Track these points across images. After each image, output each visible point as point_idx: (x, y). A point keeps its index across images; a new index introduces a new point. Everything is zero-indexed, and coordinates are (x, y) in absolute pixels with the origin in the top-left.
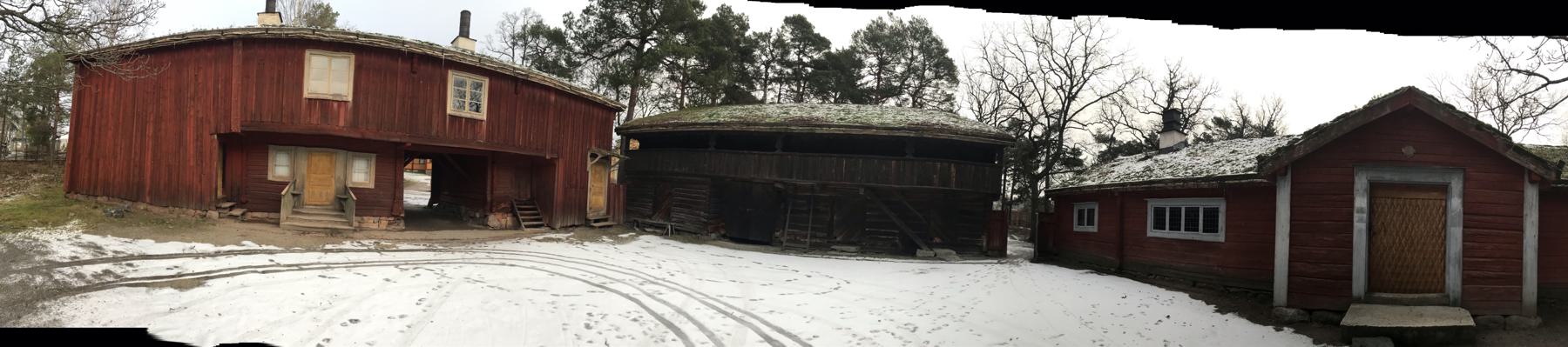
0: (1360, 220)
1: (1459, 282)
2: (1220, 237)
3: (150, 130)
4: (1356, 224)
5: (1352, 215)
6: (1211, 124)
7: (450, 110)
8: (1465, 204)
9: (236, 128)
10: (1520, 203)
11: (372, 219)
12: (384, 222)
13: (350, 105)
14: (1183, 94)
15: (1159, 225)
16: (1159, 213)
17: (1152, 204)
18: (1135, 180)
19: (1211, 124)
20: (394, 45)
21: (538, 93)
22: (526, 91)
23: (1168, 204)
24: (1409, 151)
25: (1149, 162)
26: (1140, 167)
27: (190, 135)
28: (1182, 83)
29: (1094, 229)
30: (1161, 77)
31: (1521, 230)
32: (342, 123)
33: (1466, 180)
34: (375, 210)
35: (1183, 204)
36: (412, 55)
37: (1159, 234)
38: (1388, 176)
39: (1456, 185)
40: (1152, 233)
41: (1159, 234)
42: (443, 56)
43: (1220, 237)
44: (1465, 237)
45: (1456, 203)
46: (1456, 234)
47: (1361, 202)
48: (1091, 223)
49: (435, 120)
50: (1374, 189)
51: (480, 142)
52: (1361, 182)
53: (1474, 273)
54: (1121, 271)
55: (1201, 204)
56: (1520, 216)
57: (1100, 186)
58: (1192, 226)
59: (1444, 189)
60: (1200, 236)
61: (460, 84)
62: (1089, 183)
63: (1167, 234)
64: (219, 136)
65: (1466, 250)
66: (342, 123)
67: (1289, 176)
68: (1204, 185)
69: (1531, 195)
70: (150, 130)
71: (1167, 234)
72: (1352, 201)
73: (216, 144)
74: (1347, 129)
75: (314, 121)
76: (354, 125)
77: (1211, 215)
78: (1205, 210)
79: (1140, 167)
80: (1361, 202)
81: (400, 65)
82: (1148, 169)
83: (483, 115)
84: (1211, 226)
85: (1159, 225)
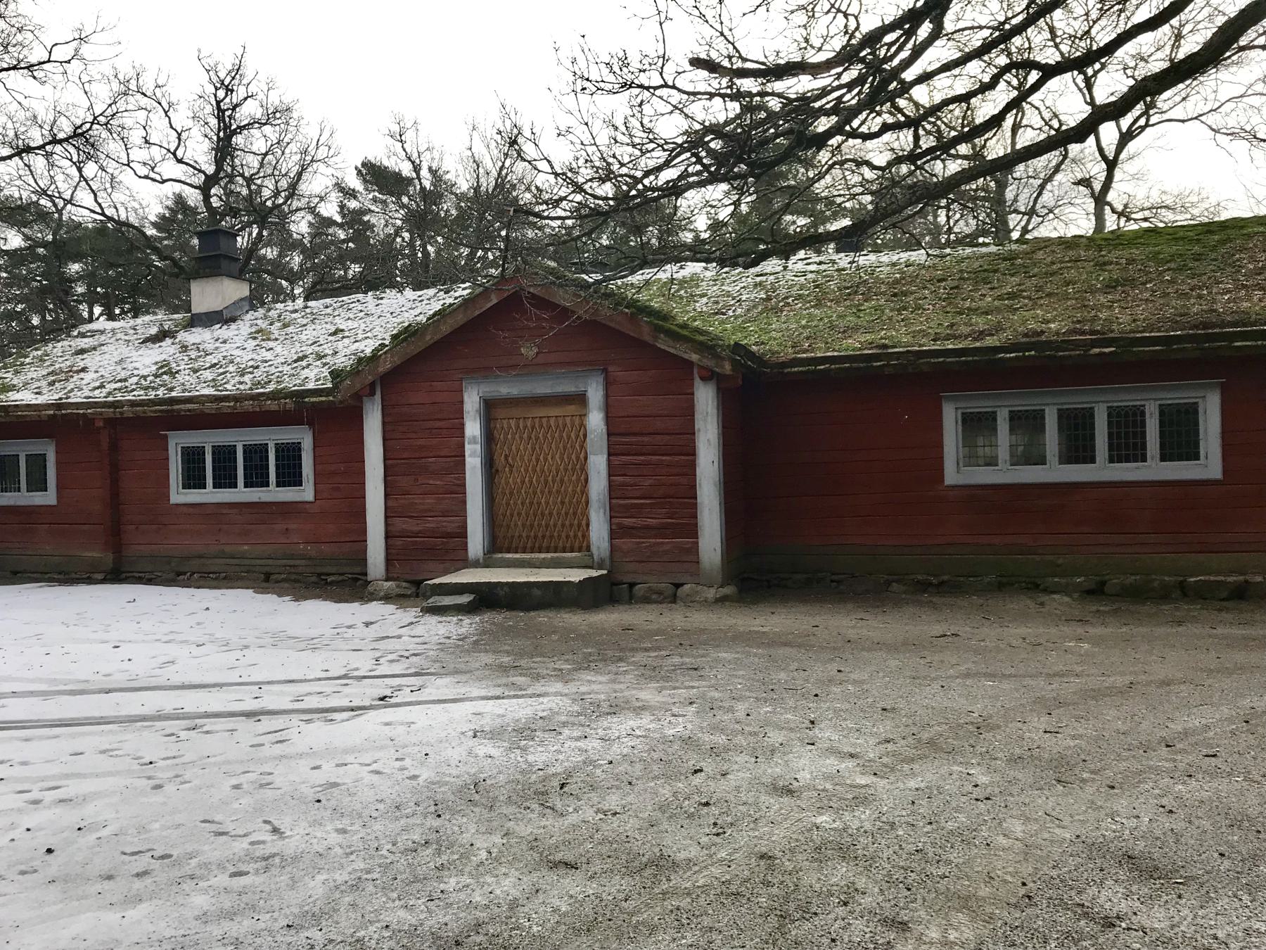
0: (472, 455)
1: (605, 534)
2: (306, 492)
4: (468, 460)
5: (462, 446)
6: (355, 183)
8: (608, 419)
10: (689, 412)
14: (257, 141)
15: (194, 479)
16: (193, 458)
17: (177, 442)
18: (139, 395)
19: (355, 183)
23: (208, 440)
24: (528, 351)
25: (167, 350)
26: (146, 360)
28: (249, 110)
29: (48, 498)
30: (189, 90)
31: (693, 453)
33: (608, 385)
35: (239, 439)
37: (194, 496)
38: (506, 389)
39: (595, 394)
40: (179, 495)
41: (194, 496)
43: (306, 492)
44: (612, 471)
45: (595, 420)
46: (598, 464)
47: (473, 428)
48: (38, 483)
50: (490, 408)
52: (472, 401)
53: (628, 521)
54: (117, 574)
55: (272, 437)
56: (689, 432)
57: (58, 406)
58: (257, 478)
59: (580, 399)
60: (274, 493)
62: (25, 397)
63: (210, 495)
65: (614, 490)
67: (378, 397)
68: (272, 405)
69: (706, 400)
71: (210, 495)
72: (461, 427)
74: (445, 329)
77: (289, 455)
78: (279, 448)
79: (146, 360)
80: (473, 428)
82: (165, 369)
84: (290, 476)
85: (194, 479)
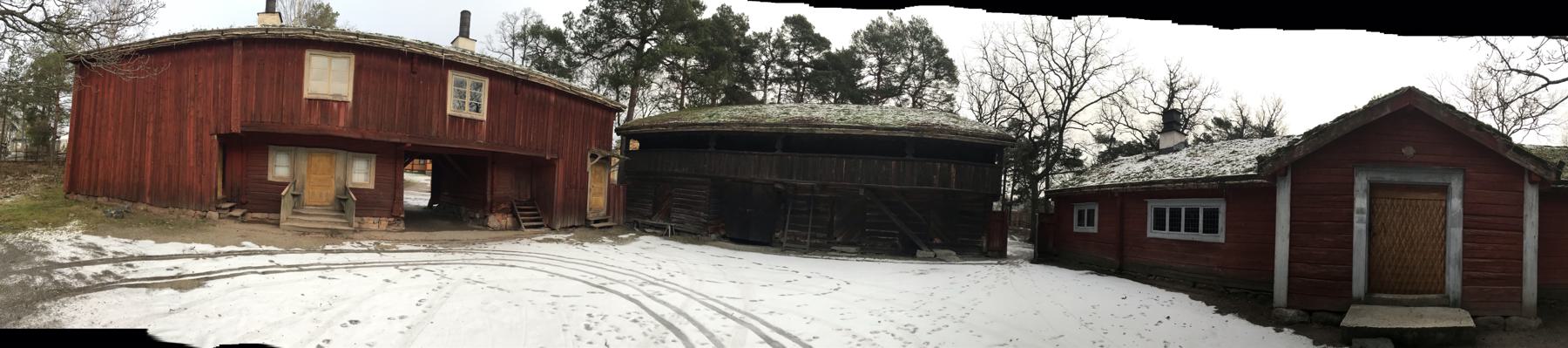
0: (1360, 221)
1: (1459, 283)
2: (1220, 237)
3: (150, 131)
4: (1356, 225)
5: (1352, 215)
6: (1211, 124)
7: (450, 110)
8: (1465, 204)
9: (236, 128)
10: (1520, 203)
11: (372, 220)
12: (384, 222)
13: (350, 106)
14: (1183, 95)
15: (1159, 225)
16: (1159, 214)
17: (1152, 205)
18: (1135, 180)
19: (1211, 124)
20: (394, 46)
21: (538, 93)
22: (526, 91)
23: (1168, 204)
24: (1409, 151)
25: (1149, 163)
26: (1140, 167)
27: (190, 136)
28: (1182, 83)
29: (1094, 230)
30: (1161, 78)
31: (1521, 230)
32: (342, 123)
33: (1466, 181)
34: (375, 211)
35: (1183, 204)
36: (412, 55)
37: (1159, 234)
38: (1388, 177)
39: (1456, 186)
40: (1152, 233)
41: (1159, 234)
42: (443, 56)
43: (1220, 237)
44: (1465, 238)
45: (1456, 204)
46: (1456, 235)
47: (1361, 203)
48: (1091, 223)
49: (435, 120)
50: (1374, 190)
51: (480, 142)
52: (1361, 183)
53: (1474, 274)
54: (1121, 272)
55: (1201, 205)
56: (1520, 217)
57: (1100, 186)
58: (1192, 226)
59: (1444, 190)
60: (1200, 236)
61: (460, 84)
62: (1089, 183)
63: (1167, 234)
64: (219, 136)
65: (1466, 251)
66: (342, 123)
67: (1289, 177)
68: (1204, 185)
69: (1531, 196)
70: (150, 131)
71: (1167, 234)
72: (1352, 202)
73: (216, 145)
74: (1347, 129)
75: (314, 122)
76: (354, 125)
77: (1211, 216)
78: (1205, 211)
79: (1140, 167)
80: (1361, 203)
81: (400, 65)
82: (1148, 169)
83: (483, 116)
84: (1211, 227)
85: (1159, 225)
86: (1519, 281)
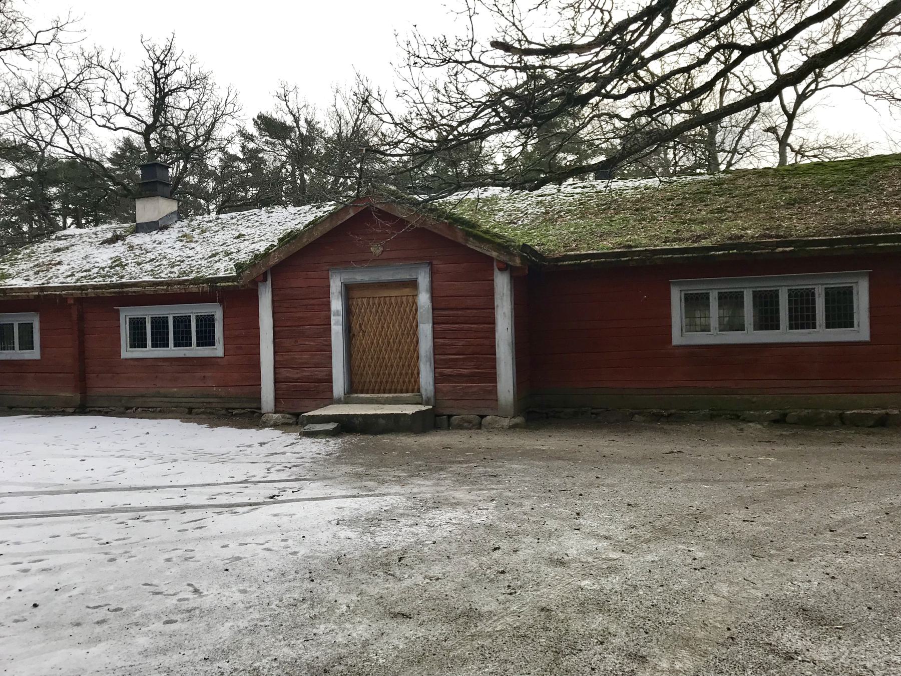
0: (336, 324)
1: (431, 380)
2: (218, 350)
4: (333, 327)
5: (329, 318)
6: (252, 130)
8: (433, 298)
10: (490, 294)
14: (183, 100)
15: (138, 341)
16: (137, 326)
17: (126, 315)
18: (99, 281)
19: (252, 130)
23: (148, 313)
24: (376, 250)
25: (119, 249)
26: (104, 256)
28: (177, 78)
29: (34, 354)
30: (135, 64)
31: (493, 322)
33: (433, 274)
35: (170, 312)
37: (138, 353)
38: (360, 277)
39: (424, 280)
40: (128, 352)
41: (138, 353)
43: (218, 350)
44: (436, 335)
45: (424, 299)
46: (426, 331)
47: (337, 305)
48: (27, 344)
50: (349, 290)
52: (336, 285)
53: (447, 371)
54: (83, 409)
55: (193, 311)
56: (491, 308)
57: (41, 289)
58: (183, 340)
59: (413, 284)
60: (195, 351)
62: (18, 282)
63: (149, 352)
65: (437, 349)
67: (269, 282)
68: (193, 288)
69: (502, 284)
71: (149, 352)
72: (328, 304)
74: (317, 234)
77: (206, 324)
78: (199, 319)
79: (104, 256)
80: (337, 305)
82: (118, 263)
84: (206, 339)
85: (138, 341)
86: (492, 377)
